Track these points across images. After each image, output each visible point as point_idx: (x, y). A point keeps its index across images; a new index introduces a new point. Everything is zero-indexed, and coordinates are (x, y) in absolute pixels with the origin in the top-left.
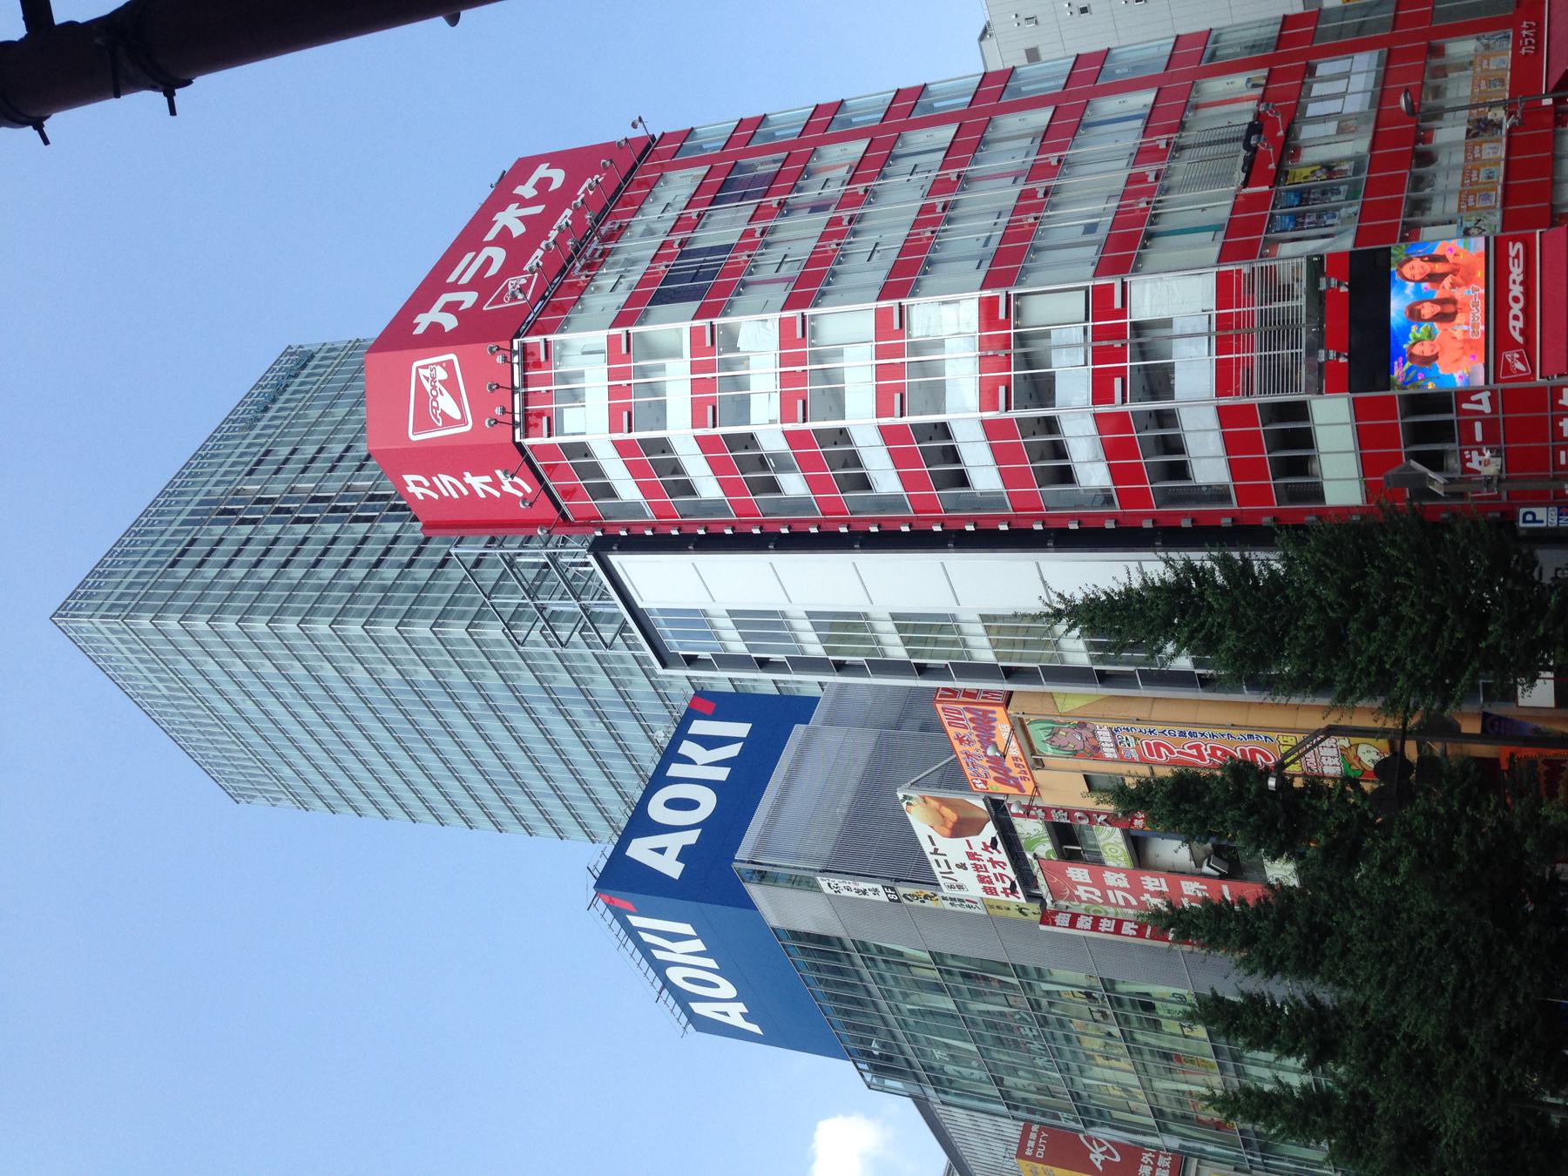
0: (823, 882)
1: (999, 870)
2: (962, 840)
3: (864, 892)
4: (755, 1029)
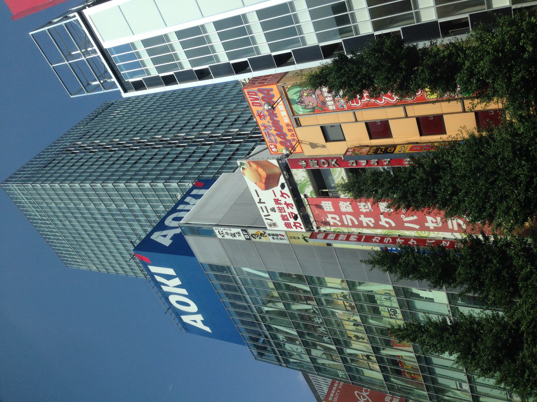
0: (216, 230)
1: (290, 210)
2: (270, 191)
3: (234, 235)
4: (207, 329)
